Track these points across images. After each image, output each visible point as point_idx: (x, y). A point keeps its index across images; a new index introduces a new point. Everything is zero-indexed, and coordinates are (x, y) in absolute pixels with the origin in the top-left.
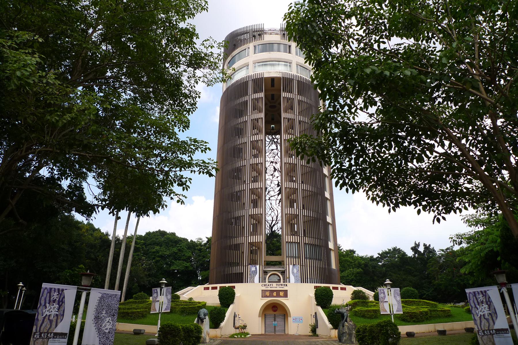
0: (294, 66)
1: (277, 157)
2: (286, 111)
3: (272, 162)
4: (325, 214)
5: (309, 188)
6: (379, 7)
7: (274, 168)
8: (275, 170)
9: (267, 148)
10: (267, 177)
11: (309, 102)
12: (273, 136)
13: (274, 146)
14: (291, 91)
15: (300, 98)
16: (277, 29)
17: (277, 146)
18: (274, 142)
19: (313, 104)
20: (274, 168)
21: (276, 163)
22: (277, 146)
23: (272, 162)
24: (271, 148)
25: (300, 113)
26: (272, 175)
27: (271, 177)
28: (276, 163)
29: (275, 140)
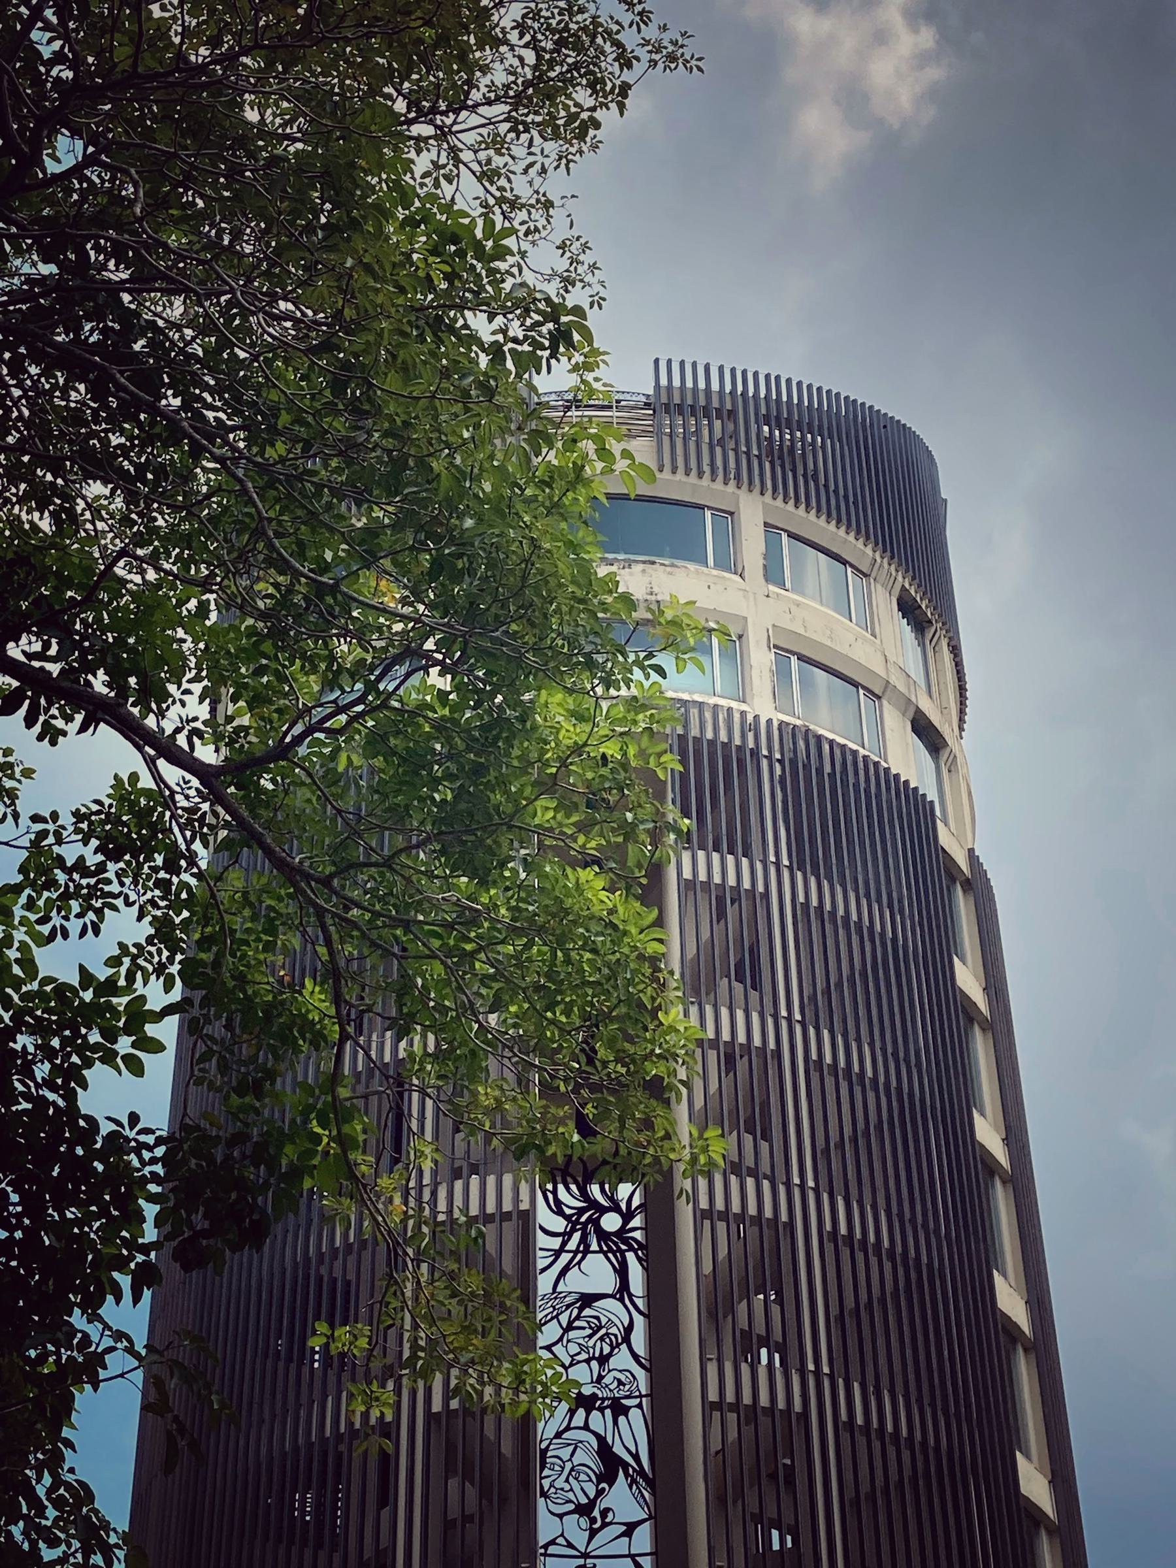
0: (761, 659)
1: (622, 1359)
2: (699, 986)
3: (587, 1403)
4: (940, 949)
5: (894, 1416)
6: (425, 1229)
7: (604, 1450)
8: (610, 1465)
9: (544, 1284)
10: (546, 1528)
11: (882, 921)
12: (595, 1190)
13: (596, 1273)
14: (735, 841)
15: (808, 889)
16: (628, 400)
17: (622, 1271)
18: (603, 1235)
19: (912, 939)
20: (604, 1450)
21: (619, 1409)
22: (622, 1271)
23: (587, 1403)
24: (575, 1283)
25: (818, 1009)
26: (583, 1510)
27: (575, 1529)
28: (619, 1409)
29: (611, 1222)
